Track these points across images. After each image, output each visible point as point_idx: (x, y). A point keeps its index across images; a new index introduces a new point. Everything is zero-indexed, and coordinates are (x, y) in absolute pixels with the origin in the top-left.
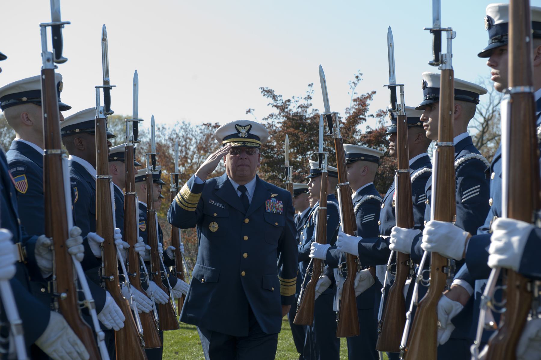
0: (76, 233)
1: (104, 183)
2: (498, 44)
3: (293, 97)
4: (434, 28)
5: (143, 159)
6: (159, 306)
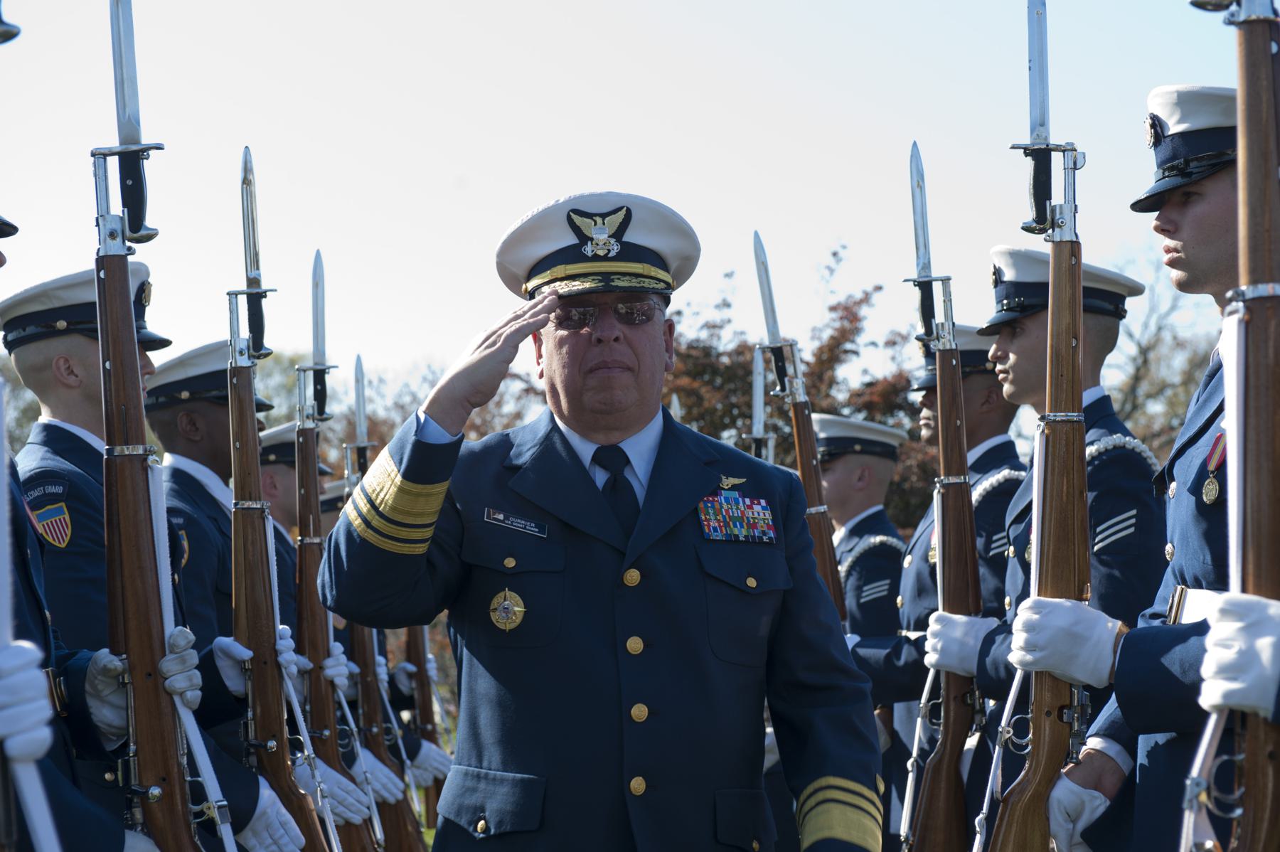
0: (182, 643)
1: (251, 520)
2: (1178, 180)
3: (688, 304)
4: (1033, 144)
5: (333, 455)
6: (382, 806)
